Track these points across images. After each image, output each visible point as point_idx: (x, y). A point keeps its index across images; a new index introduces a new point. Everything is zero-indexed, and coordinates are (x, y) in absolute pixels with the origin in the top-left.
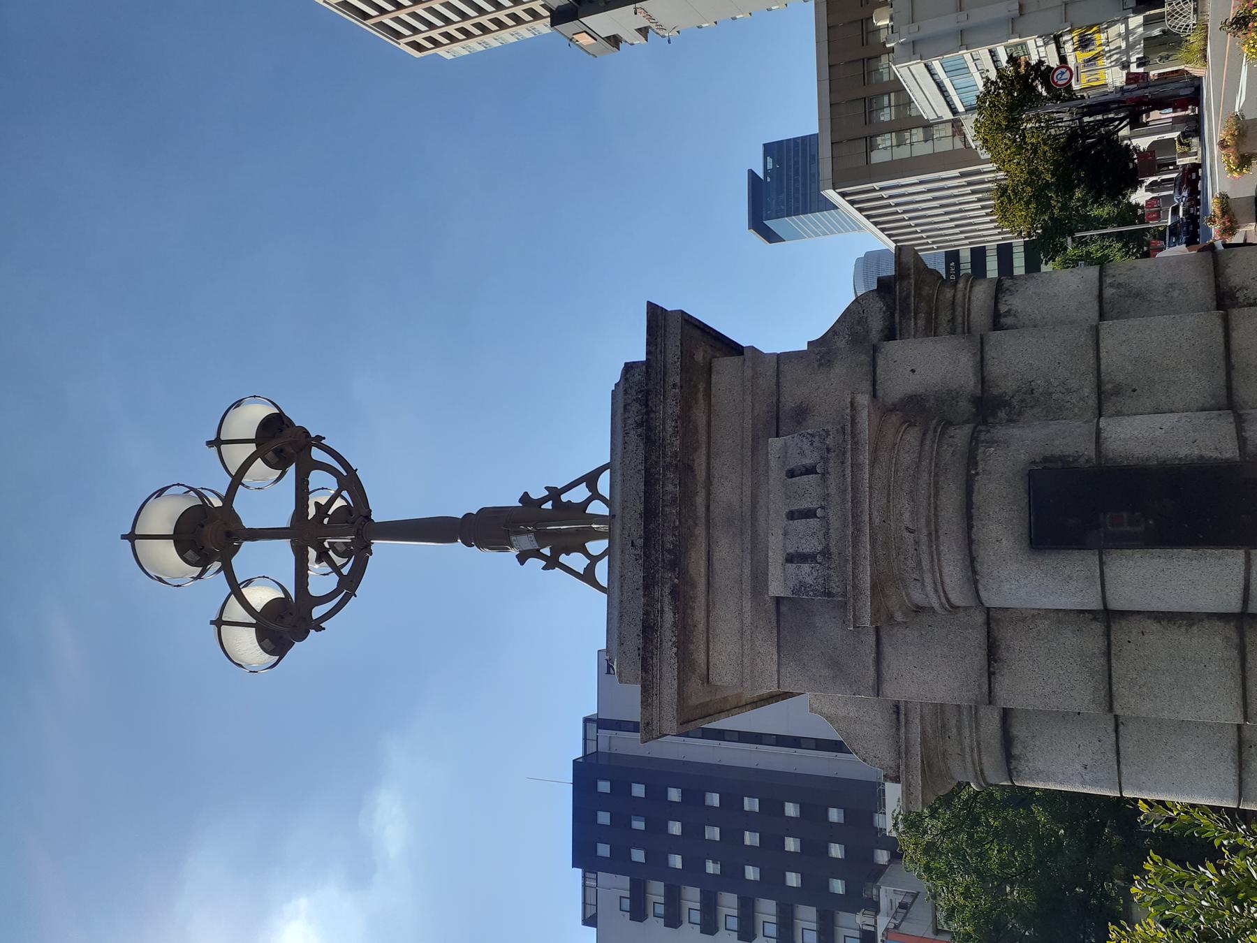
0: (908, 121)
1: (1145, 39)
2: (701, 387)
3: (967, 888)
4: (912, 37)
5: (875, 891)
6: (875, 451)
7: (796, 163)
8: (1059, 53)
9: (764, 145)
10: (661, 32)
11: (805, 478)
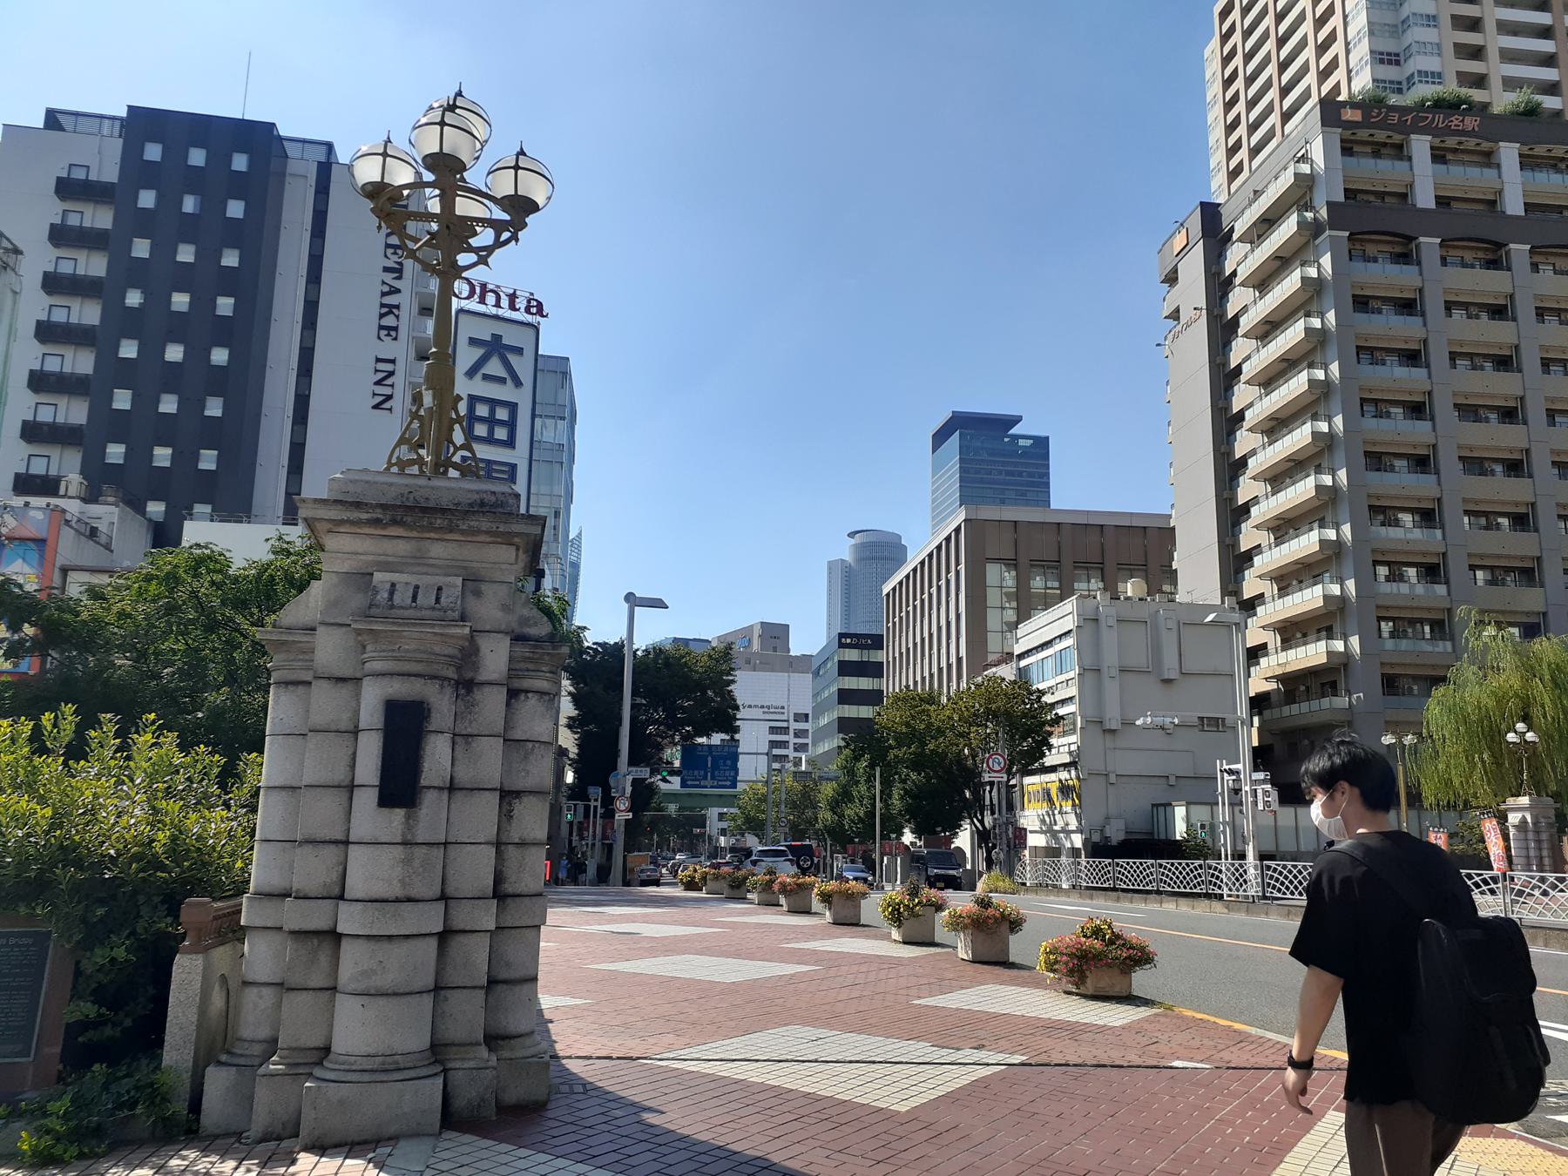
0: (1026, 606)
1: (1060, 848)
2: (499, 540)
3: (129, 616)
4: (1102, 619)
5: (111, 499)
6: (442, 634)
7: (1020, 474)
8: (1060, 765)
9: (1047, 438)
10: (1170, 337)
11: (434, 598)
